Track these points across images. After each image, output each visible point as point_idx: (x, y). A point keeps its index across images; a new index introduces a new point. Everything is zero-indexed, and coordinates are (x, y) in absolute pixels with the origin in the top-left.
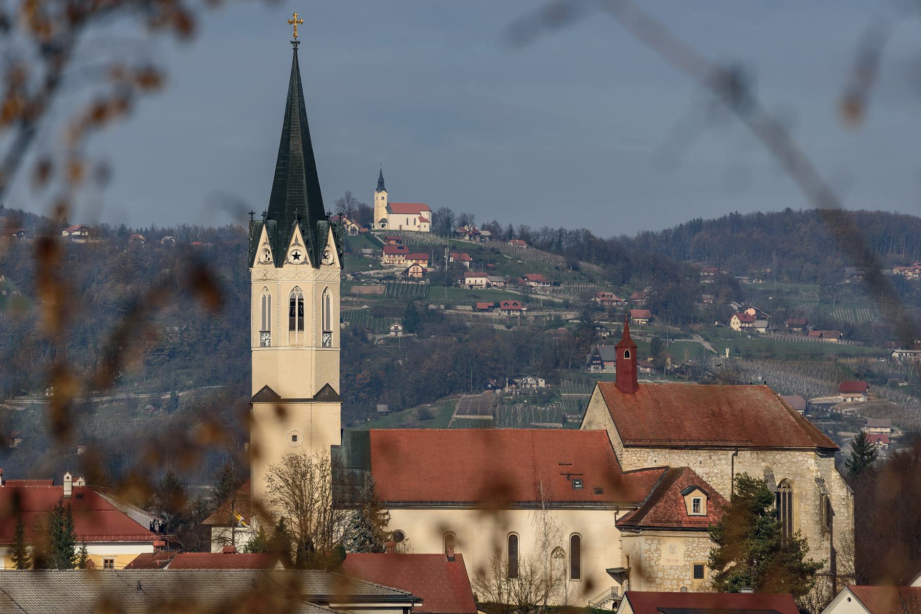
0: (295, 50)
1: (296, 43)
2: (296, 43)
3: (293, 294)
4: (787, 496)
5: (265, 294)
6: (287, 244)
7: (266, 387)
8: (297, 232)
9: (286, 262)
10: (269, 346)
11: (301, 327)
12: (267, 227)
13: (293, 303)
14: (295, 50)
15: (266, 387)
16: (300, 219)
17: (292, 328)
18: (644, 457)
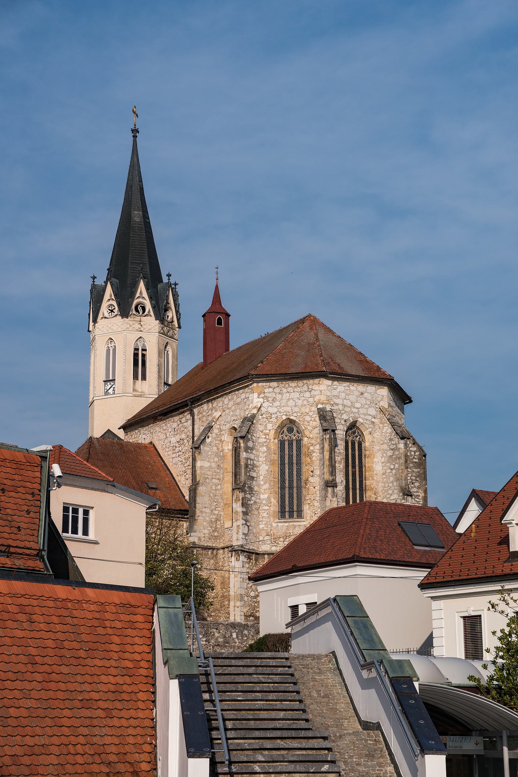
0: (135, 137)
1: (135, 131)
2: (135, 131)
3: (137, 344)
4: (357, 445)
5: (110, 345)
6: (132, 295)
7: (109, 430)
8: (142, 286)
9: (131, 313)
10: (114, 394)
11: (144, 378)
12: (111, 283)
13: (136, 355)
14: (135, 137)
15: (109, 430)
16: (144, 278)
17: (136, 377)
18: (137, 437)
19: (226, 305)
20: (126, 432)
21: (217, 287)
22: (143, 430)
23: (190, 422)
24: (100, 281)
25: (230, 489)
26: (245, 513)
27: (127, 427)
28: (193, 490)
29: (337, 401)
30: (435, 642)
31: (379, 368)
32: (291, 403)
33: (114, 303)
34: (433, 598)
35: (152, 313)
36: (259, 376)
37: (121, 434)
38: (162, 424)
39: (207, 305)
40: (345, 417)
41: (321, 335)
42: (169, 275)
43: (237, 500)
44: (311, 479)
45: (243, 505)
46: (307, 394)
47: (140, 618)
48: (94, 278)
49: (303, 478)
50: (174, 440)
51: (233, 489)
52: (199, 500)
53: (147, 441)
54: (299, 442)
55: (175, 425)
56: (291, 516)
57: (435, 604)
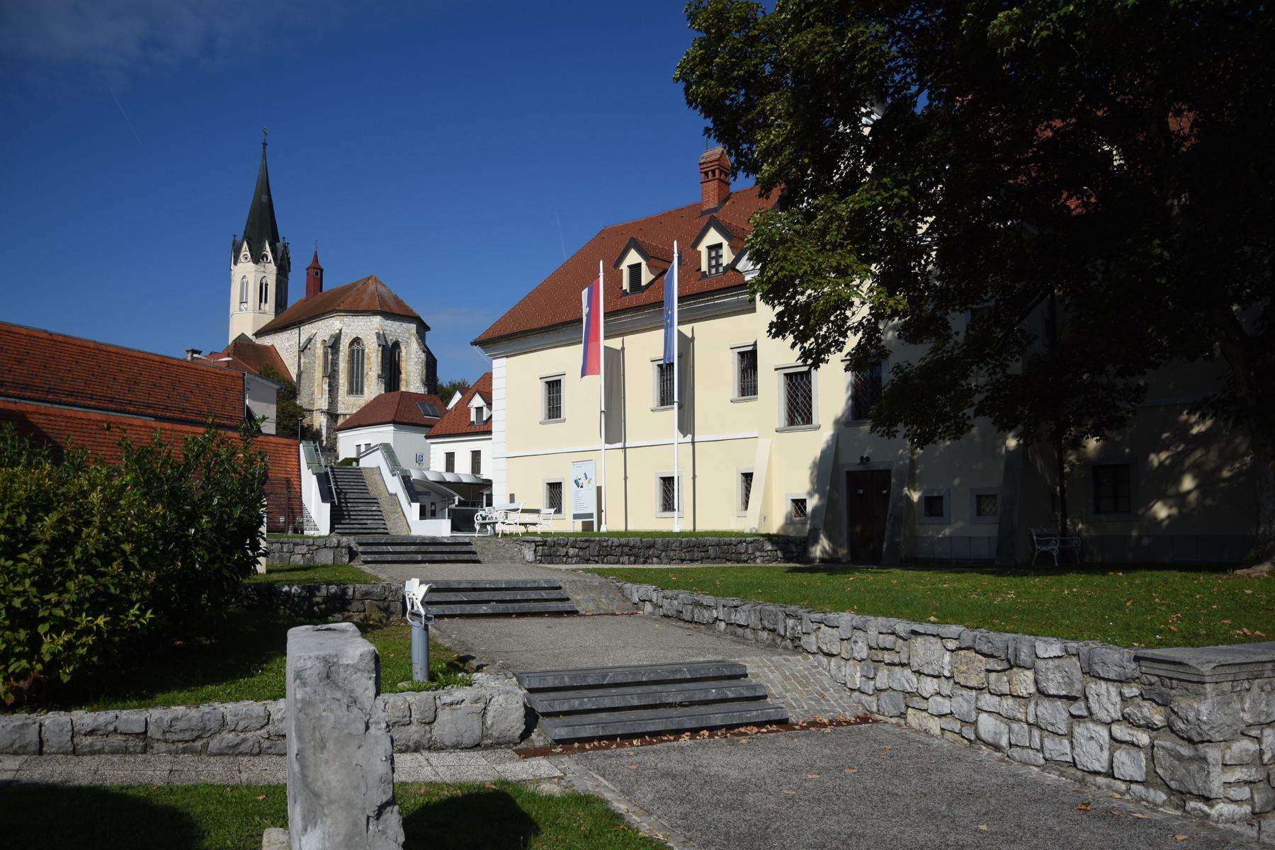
0: (265, 148)
1: (265, 144)
2: (265, 144)
11: (266, 302)
14: (265, 148)
19: (322, 264)
20: (257, 338)
21: (316, 252)
22: (267, 337)
23: (298, 335)
24: (239, 238)
25: (321, 376)
26: (330, 391)
27: (258, 334)
28: (299, 375)
29: (387, 328)
30: (493, 419)
31: (412, 311)
32: (359, 328)
33: (248, 254)
34: (432, 443)
35: (272, 261)
36: (341, 311)
37: (253, 338)
38: (280, 334)
39: (309, 262)
40: (391, 337)
41: (379, 287)
42: (284, 238)
43: (325, 383)
44: (370, 373)
45: (329, 386)
46: (369, 323)
47: (293, 450)
48: (235, 236)
49: (365, 372)
50: (287, 345)
51: (323, 377)
52: (302, 381)
53: (270, 344)
54: (363, 351)
55: (288, 336)
56: (357, 393)
57: (432, 446)
